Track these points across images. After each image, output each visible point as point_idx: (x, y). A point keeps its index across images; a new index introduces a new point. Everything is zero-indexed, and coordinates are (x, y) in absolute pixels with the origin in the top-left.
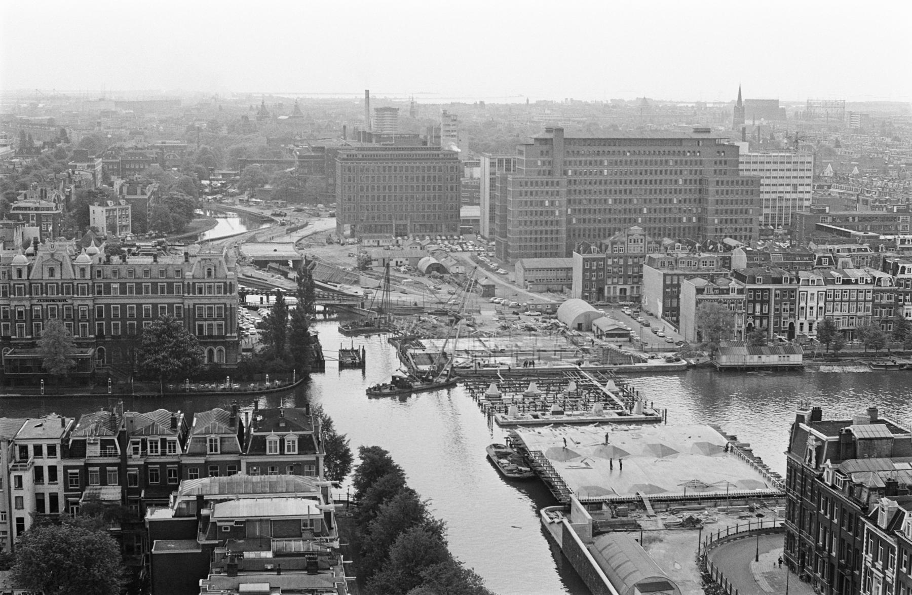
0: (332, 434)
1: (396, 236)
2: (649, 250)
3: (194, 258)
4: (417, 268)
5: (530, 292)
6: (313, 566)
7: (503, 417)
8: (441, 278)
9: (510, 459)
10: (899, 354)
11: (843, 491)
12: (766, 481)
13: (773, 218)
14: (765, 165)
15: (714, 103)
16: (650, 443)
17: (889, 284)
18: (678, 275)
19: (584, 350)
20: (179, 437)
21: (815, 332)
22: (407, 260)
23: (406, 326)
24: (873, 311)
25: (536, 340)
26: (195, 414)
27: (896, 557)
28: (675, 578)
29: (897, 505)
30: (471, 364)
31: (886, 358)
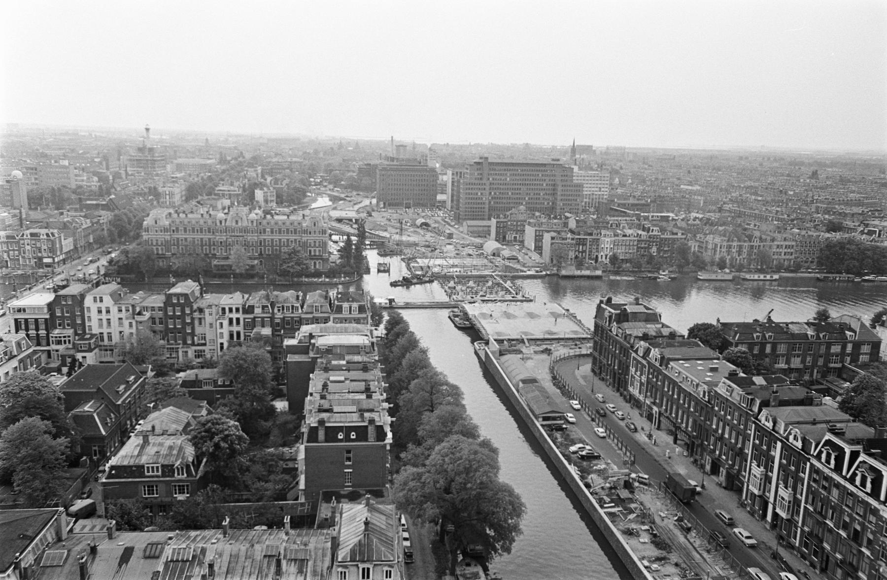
6: (365, 369)
10: (649, 272)
11: (621, 338)
12: (583, 331)
28: (539, 377)
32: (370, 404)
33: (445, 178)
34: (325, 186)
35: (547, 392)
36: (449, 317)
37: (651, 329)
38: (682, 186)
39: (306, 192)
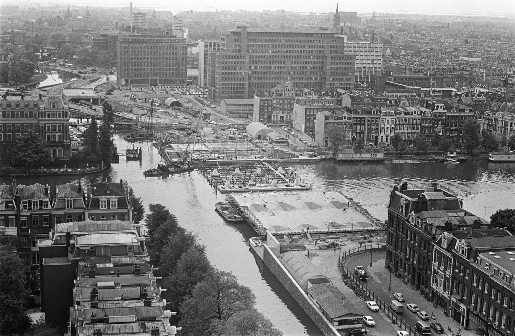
0: (132, 197)
1: (151, 85)
2: (296, 95)
3: (45, 97)
4: (165, 104)
5: (229, 117)
6: (137, 271)
7: (223, 188)
8: (179, 109)
9: (229, 211)
10: (436, 154)
11: (421, 228)
12: (371, 223)
13: (360, 78)
14: (357, 48)
15: (320, 13)
16: (306, 202)
17: (430, 115)
18: (314, 109)
19: (263, 150)
20: (49, 199)
21: (389, 141)
22: (159, 99)
23: (162, 136)
24: (421, 130)
25: (236, 145)
26: (57, 186)
27: (452, 264)
28: (328, 276)
29: (452, 236)
30: (201, 158)
31: (428, 156)
32: (151, 312)
33: (194, 50)
34: (55, 61)
35: (340, 293)
36: (216, 210)
37: (454, 217)
38: (461, 58)
39: (33, 69)
